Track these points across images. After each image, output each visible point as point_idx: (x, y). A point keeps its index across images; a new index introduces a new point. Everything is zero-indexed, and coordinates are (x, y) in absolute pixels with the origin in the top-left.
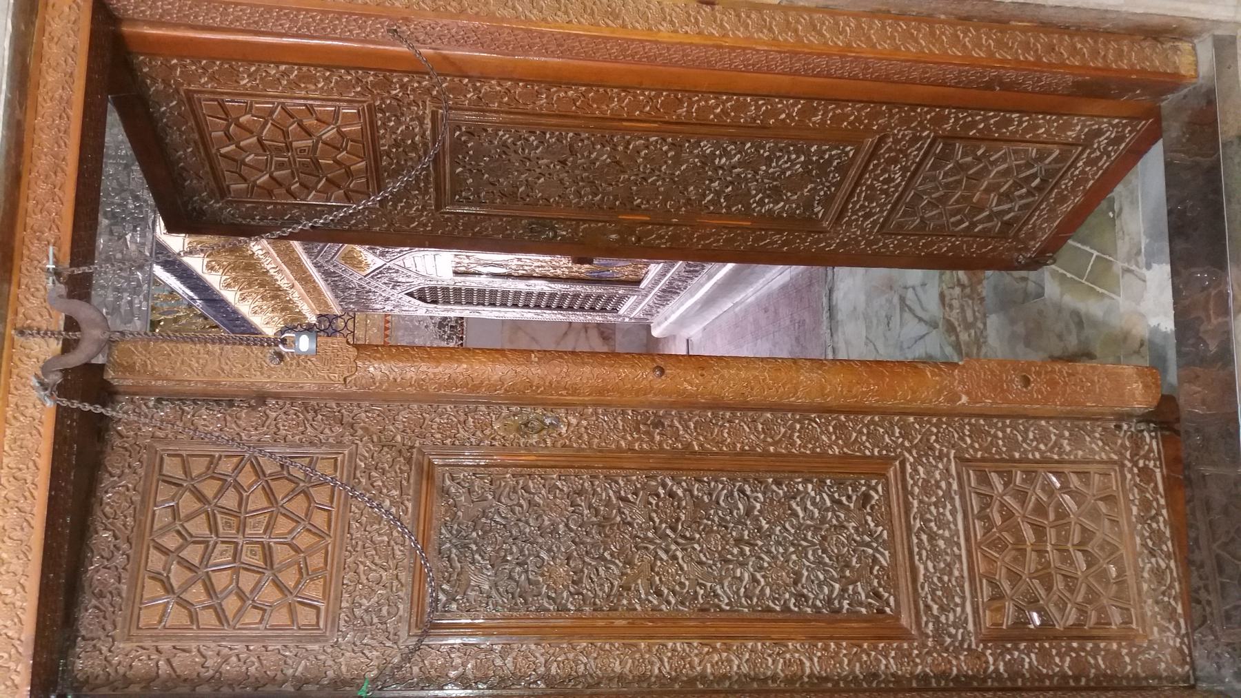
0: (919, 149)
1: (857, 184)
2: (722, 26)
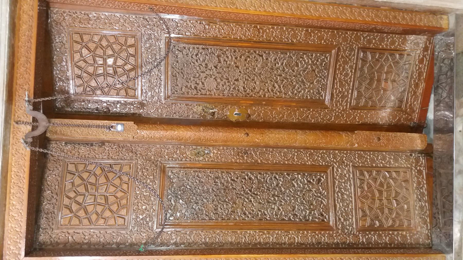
0: (354, 55)
1: (334, 78)
2: (273, 9)
